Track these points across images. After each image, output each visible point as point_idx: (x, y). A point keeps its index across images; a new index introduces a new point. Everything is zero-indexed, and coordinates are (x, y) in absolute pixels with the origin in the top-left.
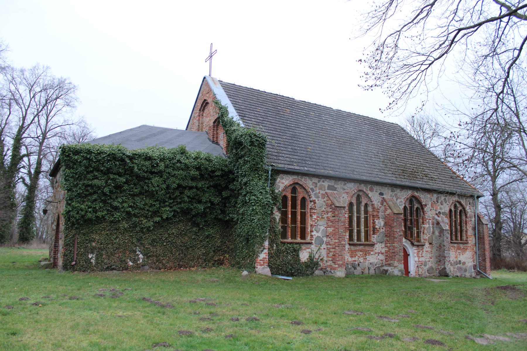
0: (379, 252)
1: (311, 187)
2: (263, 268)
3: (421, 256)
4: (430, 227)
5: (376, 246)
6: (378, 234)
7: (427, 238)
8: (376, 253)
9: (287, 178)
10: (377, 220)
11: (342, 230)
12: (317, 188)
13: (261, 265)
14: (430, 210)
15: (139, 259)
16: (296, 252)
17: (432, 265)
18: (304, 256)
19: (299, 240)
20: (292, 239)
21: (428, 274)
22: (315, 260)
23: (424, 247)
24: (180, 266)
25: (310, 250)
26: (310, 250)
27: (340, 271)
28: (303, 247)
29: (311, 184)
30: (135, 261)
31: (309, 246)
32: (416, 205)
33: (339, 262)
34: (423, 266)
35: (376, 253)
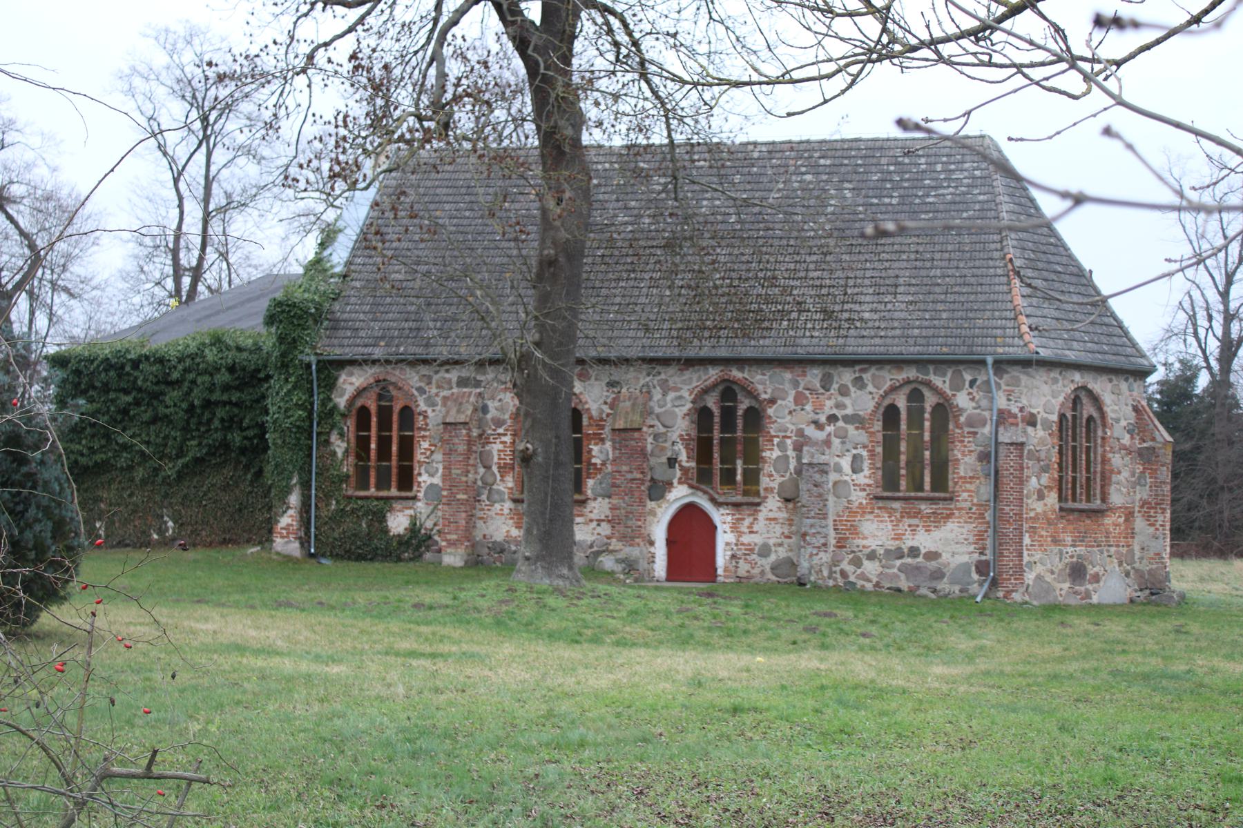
0: (603, 517)
1: (418, 385)
2: (287, 543)
3: (747, 530)
4: (787, 457)
5: (591, 504)
6: (599, 477)
7: (775, 485)
8: (591, 521)
9: (361, 372)
10: (596, 444)
11: (459, 472)
12: (434, 386)
13: (282, 537)
14: (790, 412)
15: (167, 530)
16: (379, 517)
17: (790, 554)
18: (398, 523)
19: (394, 492)
20: (378, 488)
21: (774, 578)
22: (423, 531)
23: (761, 508)
24: (225, 542)
25: (411, 512)
26: (411, 512)
27: (450, 554)
28: (397, 506)
29: (417, 378)
30: (161, 532)
31: (410, 503)
32: (744, 404)
33: (449, 537)
34: (754, 556)
35: (591, 521)
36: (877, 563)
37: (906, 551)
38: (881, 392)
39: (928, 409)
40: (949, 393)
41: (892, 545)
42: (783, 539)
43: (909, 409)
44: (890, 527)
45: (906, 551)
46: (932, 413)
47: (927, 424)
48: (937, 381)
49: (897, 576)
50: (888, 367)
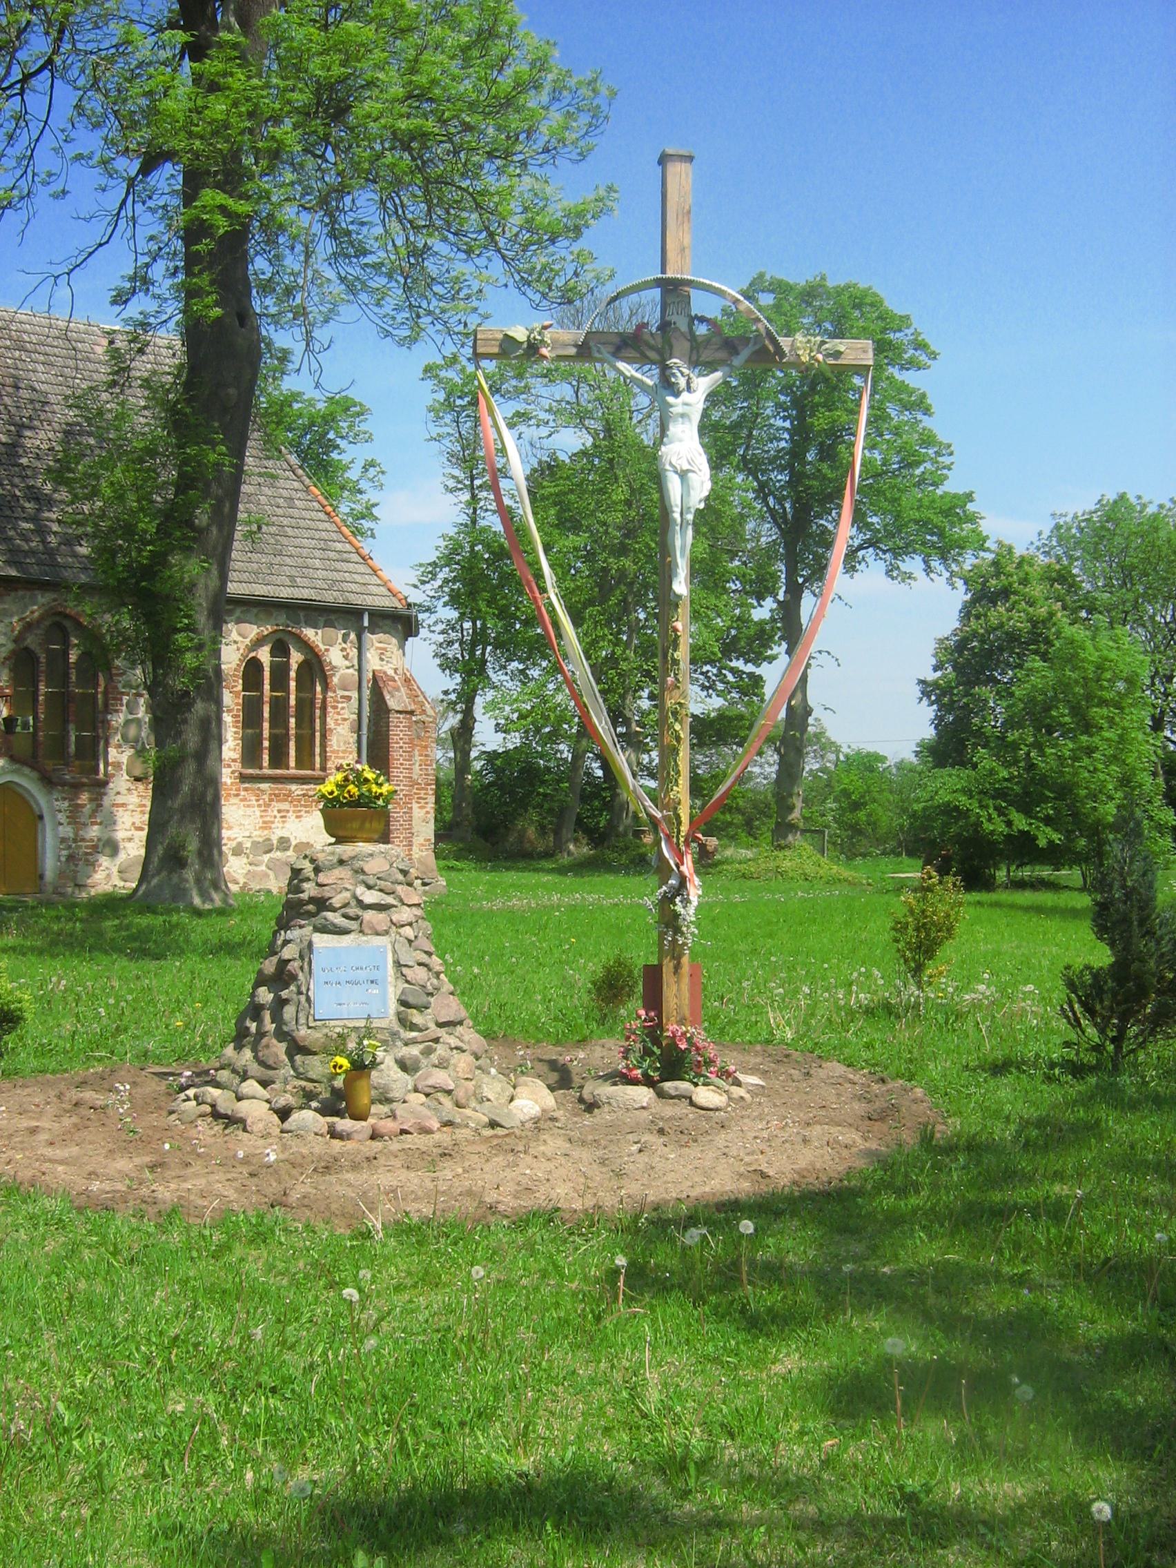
36: (245, 860)
37: (275, 842)
38: (247, 641)
39: (294, 666)
40: (322, 647)
41: (259, 835)
42: (133, 832)
43: (272, 664)
44: (258, 814)
45: (275, 842)
46: (298, 672)
47: (293, 684)
48: (310, 633)
49: (267, 875)
50: (255, 610)
